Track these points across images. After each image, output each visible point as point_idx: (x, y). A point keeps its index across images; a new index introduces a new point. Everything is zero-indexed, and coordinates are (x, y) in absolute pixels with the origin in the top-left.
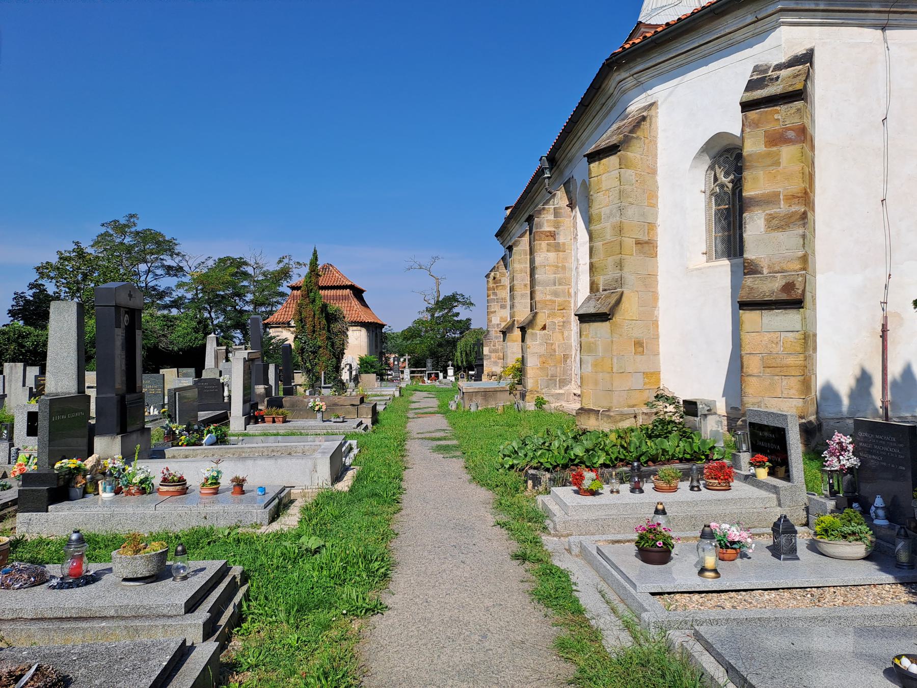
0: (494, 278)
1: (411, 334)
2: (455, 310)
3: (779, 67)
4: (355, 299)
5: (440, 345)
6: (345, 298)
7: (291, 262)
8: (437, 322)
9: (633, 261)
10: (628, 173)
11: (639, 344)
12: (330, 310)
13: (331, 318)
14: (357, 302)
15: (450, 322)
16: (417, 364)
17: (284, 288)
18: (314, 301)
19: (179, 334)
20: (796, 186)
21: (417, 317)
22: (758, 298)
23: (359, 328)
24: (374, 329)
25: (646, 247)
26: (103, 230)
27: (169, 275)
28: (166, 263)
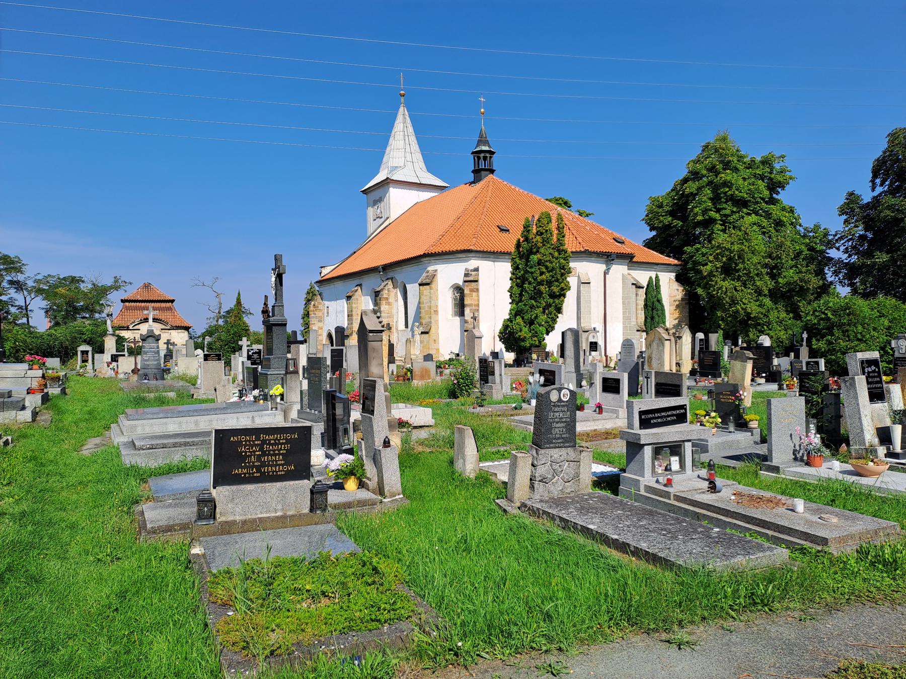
0: (314, 305)
3: (471, 271)
9: (433, 316)
10: (432, 291)
11: (435, 340)
20: (476, 303)
22: (162, 298)
23: (183, 331)
25: (278, 257)
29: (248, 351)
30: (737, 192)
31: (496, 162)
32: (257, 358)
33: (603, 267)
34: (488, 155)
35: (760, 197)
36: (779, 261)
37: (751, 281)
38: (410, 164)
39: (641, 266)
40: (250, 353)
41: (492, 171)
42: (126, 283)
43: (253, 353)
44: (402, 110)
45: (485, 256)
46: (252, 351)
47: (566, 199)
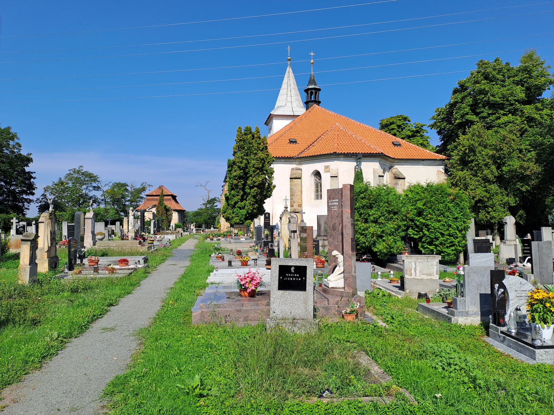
1: (197, 214)
2: (215, 204)
4: (173, 200)
5: (209, 219)
6: (169, 200)
7: (146, 185)
8: (207, 209)
12: (167, 208)
13: (167, 210)
14: (174, 201)
15: (213, 209)
16: (199, 226)
17: (143, 195)
18: (162, 205)
19: (110, 215)
21: (199, 207)
24: (182, 213)
26: (68, 172)
27: (95, 190)
28: (93, 185)
29: (17, 226)
30: (491, 98)
31: (321, 96)
32: (22, 230)
33: (355, 164)
34: (313, 91)
35: (514, 100)
36: (502, 152)
37: (480, 171)
38: (289, 104)
39: (407, 162)
40: (18, 227)
41: (318, 103)
42: (150, 186)
43: (19, 227)
44: (289, 70)
45: (312, 159)
46: (19, 226)
47: (405, 115)
